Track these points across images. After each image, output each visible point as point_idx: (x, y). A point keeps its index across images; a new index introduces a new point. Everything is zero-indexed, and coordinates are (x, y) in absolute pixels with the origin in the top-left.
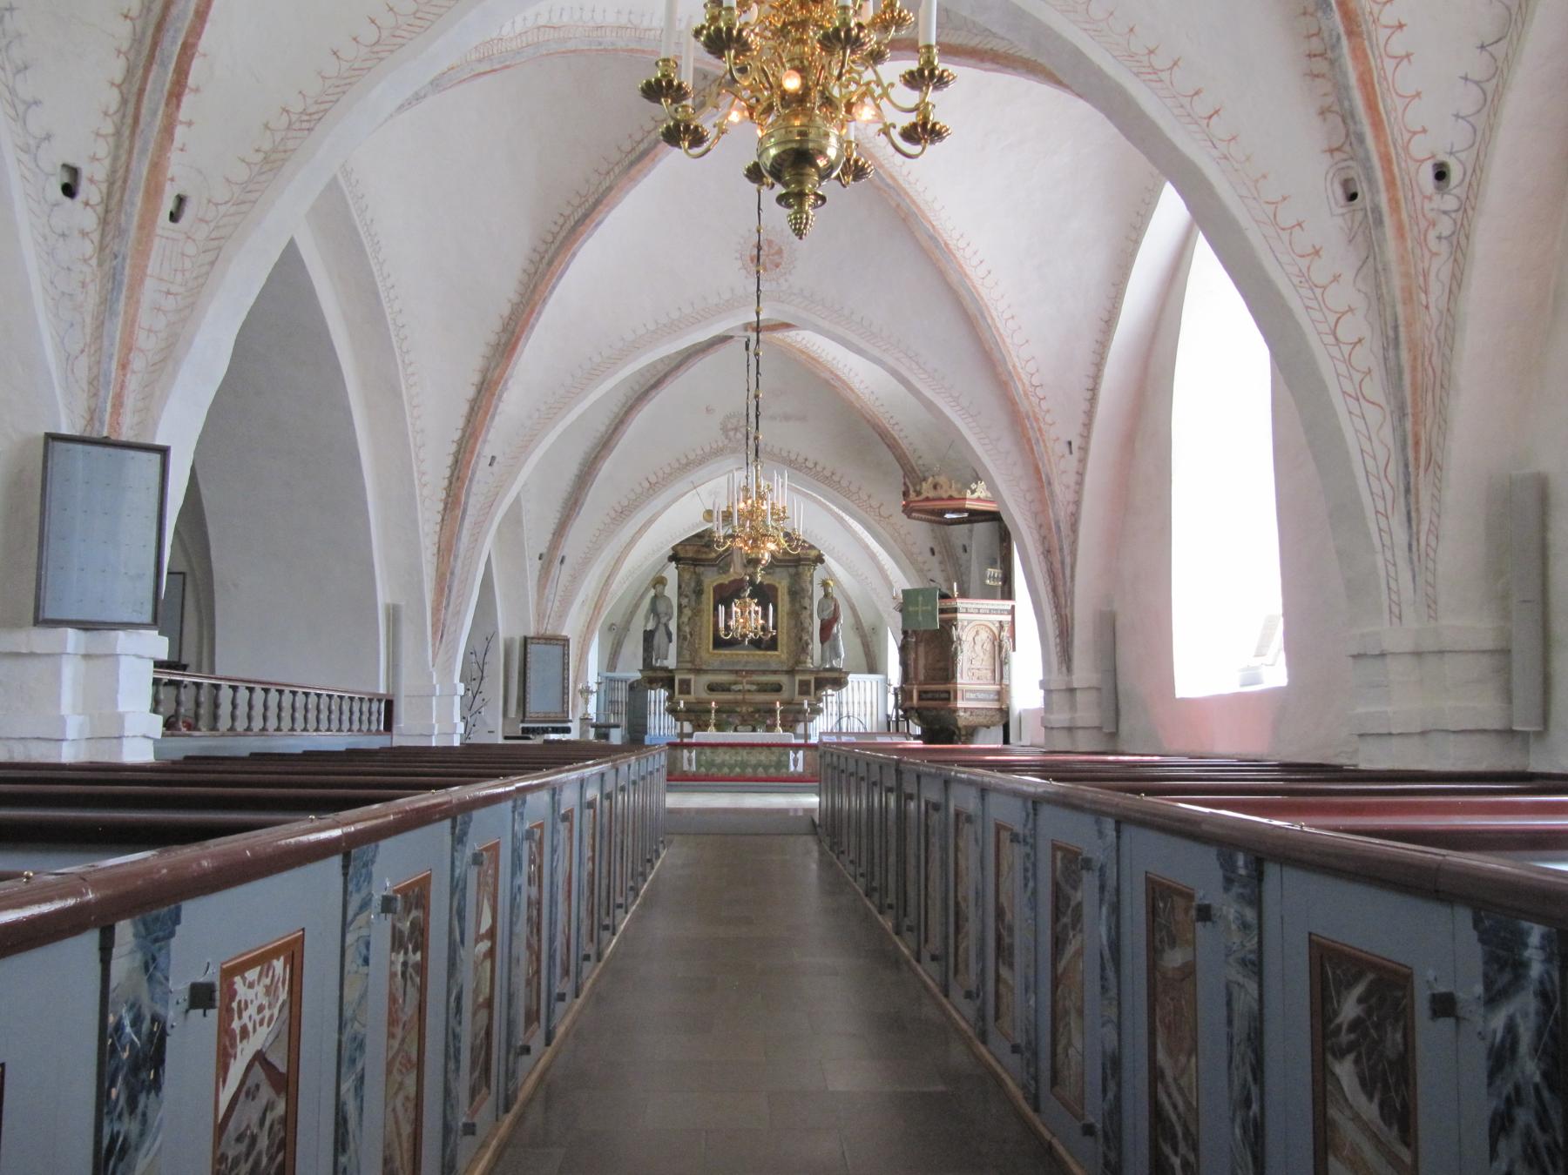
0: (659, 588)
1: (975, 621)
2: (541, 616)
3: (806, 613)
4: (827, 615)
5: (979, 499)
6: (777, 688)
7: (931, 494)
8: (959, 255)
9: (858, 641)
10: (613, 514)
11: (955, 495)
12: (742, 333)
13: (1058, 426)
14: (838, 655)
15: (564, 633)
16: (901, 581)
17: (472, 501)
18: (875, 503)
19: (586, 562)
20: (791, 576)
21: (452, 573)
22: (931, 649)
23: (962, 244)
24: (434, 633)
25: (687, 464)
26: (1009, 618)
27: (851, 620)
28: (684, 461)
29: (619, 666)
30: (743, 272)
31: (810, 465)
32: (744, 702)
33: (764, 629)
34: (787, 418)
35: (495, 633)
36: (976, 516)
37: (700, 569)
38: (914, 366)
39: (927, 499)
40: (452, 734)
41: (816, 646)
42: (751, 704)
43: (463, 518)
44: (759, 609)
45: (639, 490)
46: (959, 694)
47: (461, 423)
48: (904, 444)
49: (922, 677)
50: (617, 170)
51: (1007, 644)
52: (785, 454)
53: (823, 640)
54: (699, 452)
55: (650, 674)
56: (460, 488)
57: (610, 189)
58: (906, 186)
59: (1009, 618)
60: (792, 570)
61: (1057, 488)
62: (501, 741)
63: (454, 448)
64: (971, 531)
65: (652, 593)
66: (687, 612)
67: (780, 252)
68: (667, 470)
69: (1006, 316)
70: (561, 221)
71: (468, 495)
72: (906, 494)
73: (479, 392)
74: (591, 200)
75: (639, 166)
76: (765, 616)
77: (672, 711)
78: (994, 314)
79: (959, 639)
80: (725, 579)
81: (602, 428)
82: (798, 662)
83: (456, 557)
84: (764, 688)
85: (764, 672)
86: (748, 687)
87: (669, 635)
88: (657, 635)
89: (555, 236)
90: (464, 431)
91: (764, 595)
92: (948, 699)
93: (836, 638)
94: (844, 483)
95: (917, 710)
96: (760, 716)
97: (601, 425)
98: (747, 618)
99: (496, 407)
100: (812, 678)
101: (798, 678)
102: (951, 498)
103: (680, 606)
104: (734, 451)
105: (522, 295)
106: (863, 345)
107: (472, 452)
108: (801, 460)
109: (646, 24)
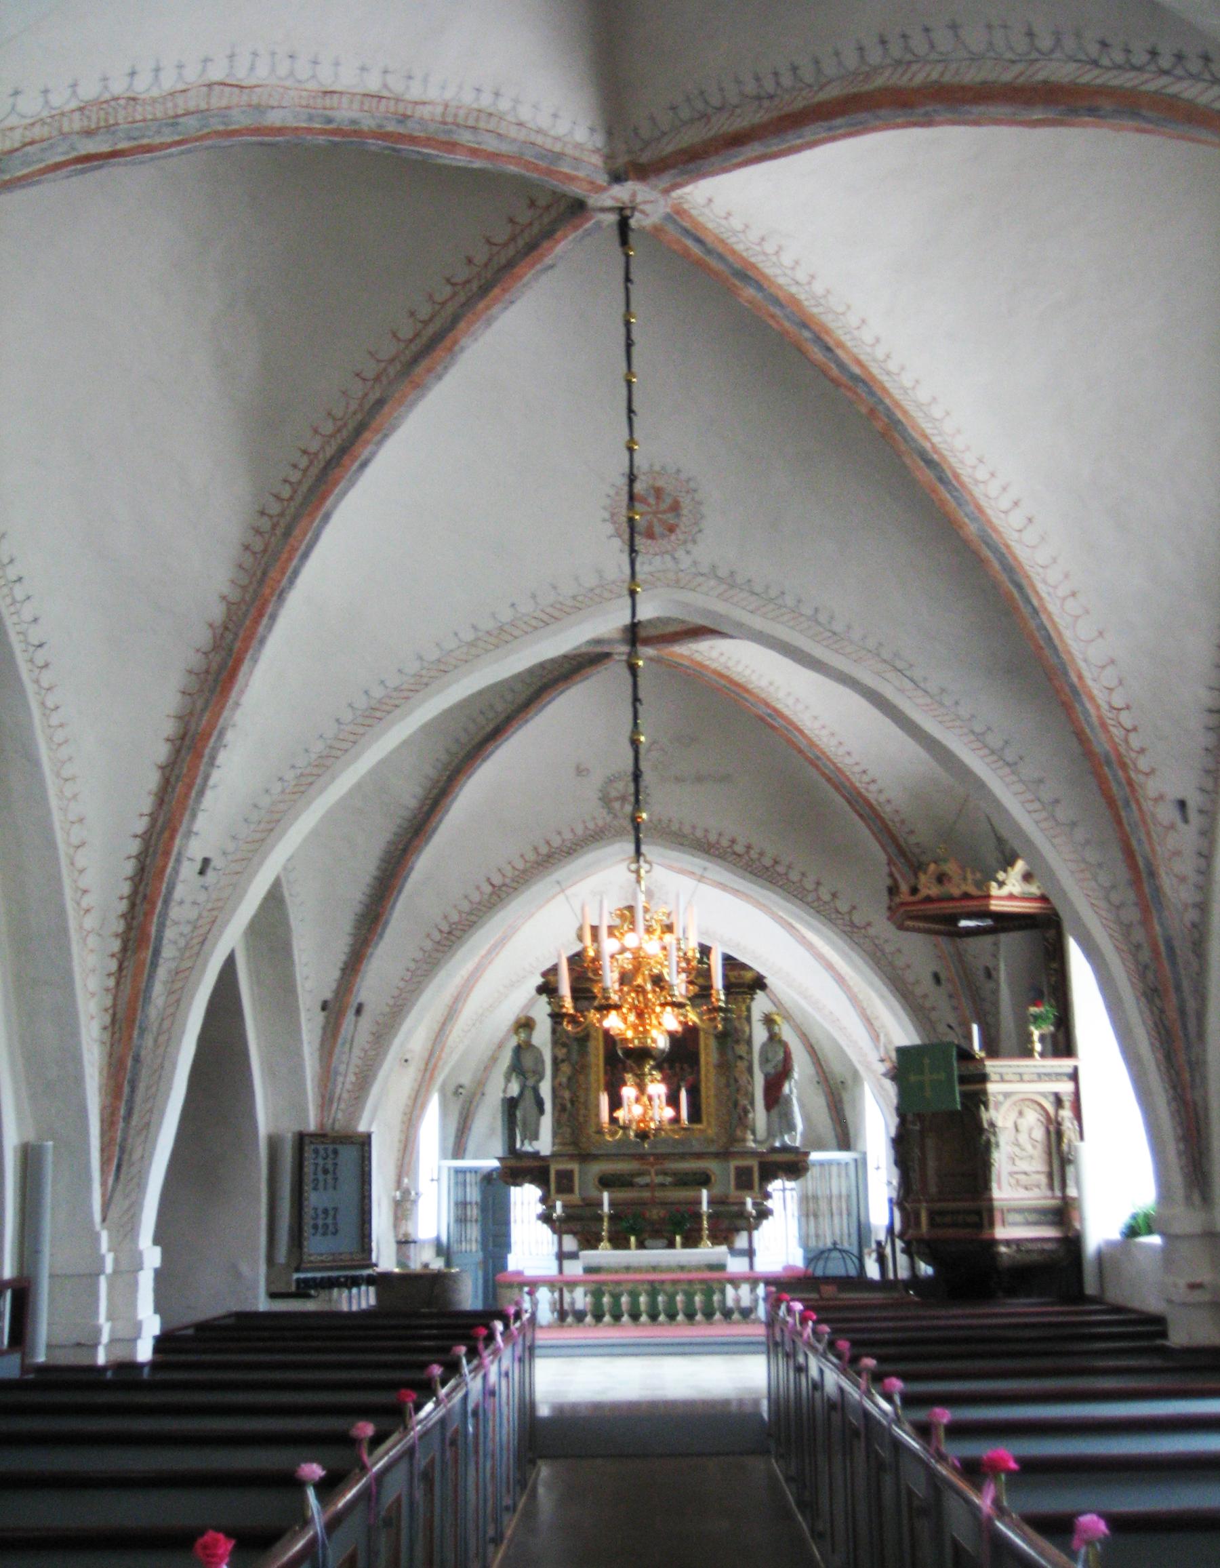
1: (1015, 1096)
2: (326, 1101)
3: (742, 1065)
5: (1011, 897)
7: (934, 891)
8: (978, 491)
10: (437, 936)
11: (972, 890)
14: (791, 1127)
15: (362, 1128)
16: (901, 1032)
17: (170, 933)
18: (844, 907)
19: (398, 1010)
21: (137, 1059)
22: (944, 1136)
23: (981, 474)
24: (105, 1163)
25: (549, 856)
27: (810, 1070)
28: (544, 850)
31: (739, 848)
32: (653, 1202)
33: (676, 1120)
34: (699, 779)
36: (1005, 922)
38: (908, 685)
39: (928, 899)
40: (133, 1340)
41: (759, 1116)
42: (663, 1204)
43: (154, 965)
46: (998, 1217)
48: (887, 811)
49: (933, 1189)
50: (392, 371)
51: (1069, 1126)
52: (699, 833)
53: (769, 1106)
54: (568, 835)
56: (148, 914)
57: (380, 402)
58: (883, 378)
61: (1167, 882)
62: (263, 1304)
63: (134, 847)
64: (996, 944)
65: (514, 1041)
66: (566, 1068)
67: (675, 507)
69: (1061, 592)
70: (304, 462)
71: (162, 927)
73: (178, 751)
74: (351, 425)
75: (425, 363)
77: (546, 1218)
79: (992, 1125)
81: (413, 803)
82: (734, 1140)
83: (143, 1031)
85: (683, 1156)
88: (522, 1105)
89: (295, 487)
90: (153, 817)
93: (788, 1100)
96: (681, 1227)
97: (408, 793)
98: (647, 1104)
99: (207, 778)
100: (754, 1163)
101: (734, 1164)
102: (966, 896)
103: (556, 1062)
104: (618, 834)
105: (244, 588)
106: (818, 651)
107: (167, 854)
108: (725, 842)
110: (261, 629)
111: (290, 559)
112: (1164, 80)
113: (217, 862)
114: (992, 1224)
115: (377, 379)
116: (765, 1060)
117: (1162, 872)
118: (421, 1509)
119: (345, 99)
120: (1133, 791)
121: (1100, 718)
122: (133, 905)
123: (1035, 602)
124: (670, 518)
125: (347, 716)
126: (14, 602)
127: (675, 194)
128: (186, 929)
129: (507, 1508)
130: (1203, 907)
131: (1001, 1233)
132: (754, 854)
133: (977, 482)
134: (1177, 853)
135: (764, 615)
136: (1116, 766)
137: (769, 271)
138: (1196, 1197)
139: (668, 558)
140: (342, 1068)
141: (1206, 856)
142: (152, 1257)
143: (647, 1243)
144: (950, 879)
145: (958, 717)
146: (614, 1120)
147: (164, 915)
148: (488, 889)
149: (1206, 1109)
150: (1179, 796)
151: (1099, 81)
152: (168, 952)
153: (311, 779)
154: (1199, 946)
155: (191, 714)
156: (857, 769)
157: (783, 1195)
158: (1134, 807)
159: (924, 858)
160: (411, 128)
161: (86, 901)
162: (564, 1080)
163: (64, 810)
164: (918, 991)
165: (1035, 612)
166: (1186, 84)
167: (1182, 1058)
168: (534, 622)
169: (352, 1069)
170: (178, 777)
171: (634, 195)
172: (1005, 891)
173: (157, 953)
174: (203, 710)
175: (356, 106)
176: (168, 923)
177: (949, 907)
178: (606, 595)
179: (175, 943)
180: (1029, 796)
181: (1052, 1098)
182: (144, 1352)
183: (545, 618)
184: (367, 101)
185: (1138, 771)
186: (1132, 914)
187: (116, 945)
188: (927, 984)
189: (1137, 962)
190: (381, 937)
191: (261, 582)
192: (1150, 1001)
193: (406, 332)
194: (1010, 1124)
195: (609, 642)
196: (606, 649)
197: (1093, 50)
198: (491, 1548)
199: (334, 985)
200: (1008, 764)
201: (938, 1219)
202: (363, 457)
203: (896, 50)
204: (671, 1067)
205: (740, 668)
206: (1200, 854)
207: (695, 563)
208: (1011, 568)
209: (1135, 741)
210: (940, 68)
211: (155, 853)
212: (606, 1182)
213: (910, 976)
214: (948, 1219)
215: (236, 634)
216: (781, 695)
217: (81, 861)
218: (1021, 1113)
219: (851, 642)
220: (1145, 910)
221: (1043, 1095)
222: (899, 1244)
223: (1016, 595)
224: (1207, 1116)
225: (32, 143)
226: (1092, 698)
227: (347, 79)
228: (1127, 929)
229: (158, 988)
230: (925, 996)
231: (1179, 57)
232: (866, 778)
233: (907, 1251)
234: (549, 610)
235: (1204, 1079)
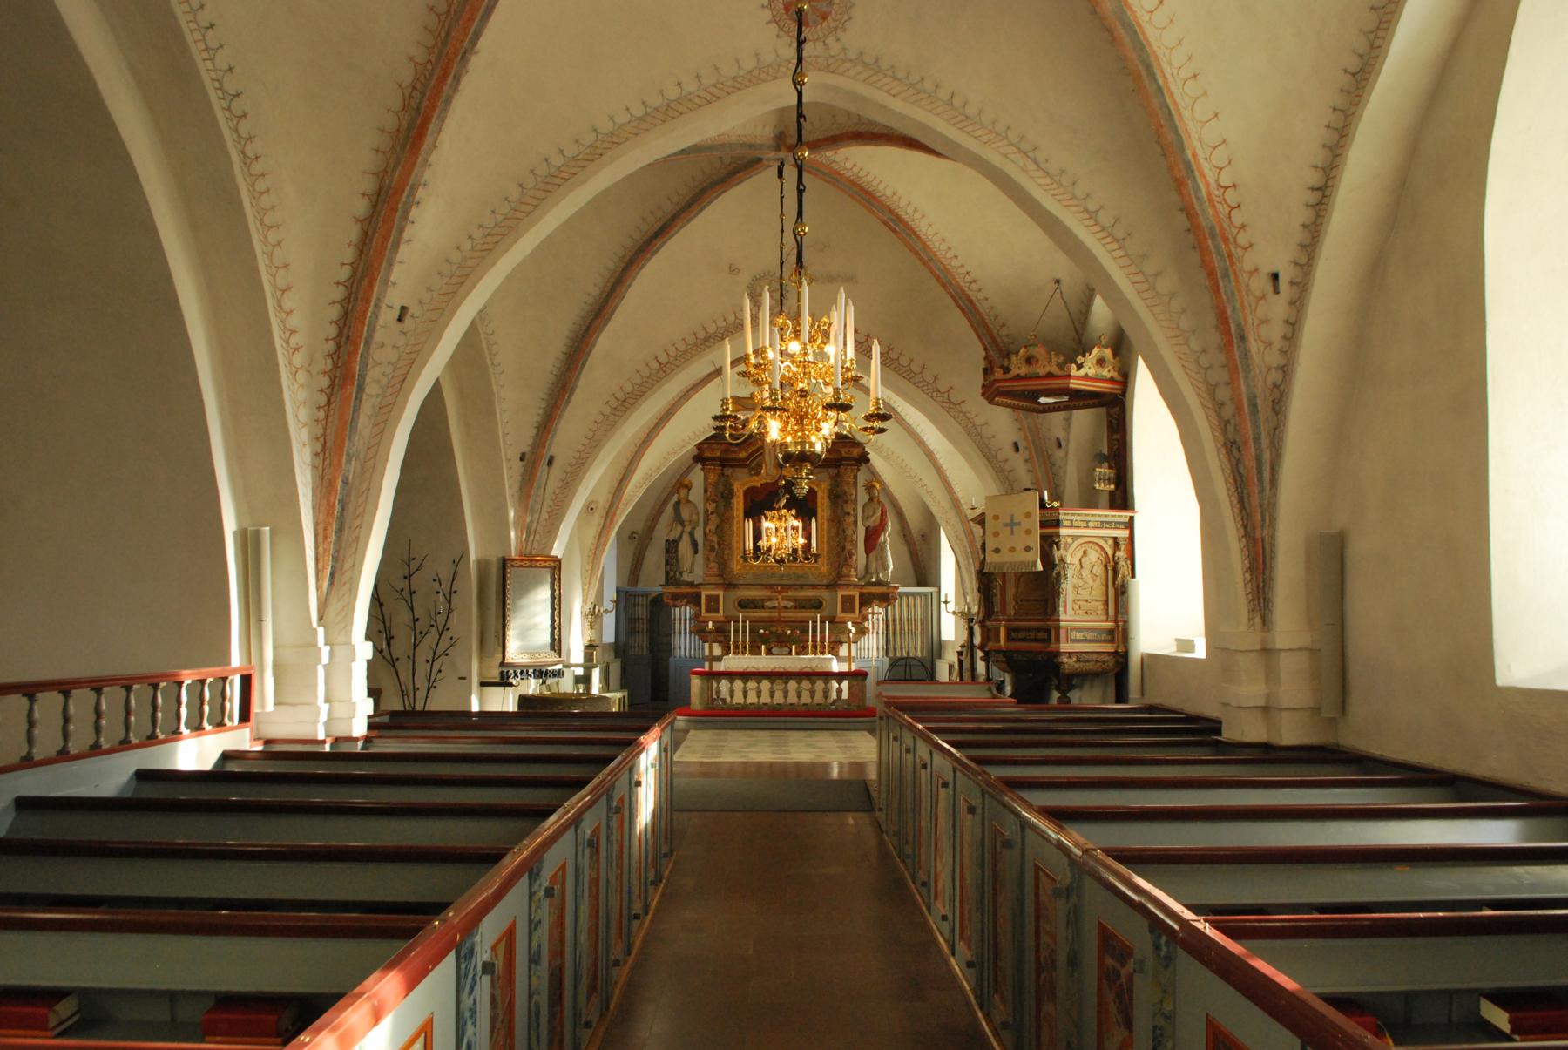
0: (683, 492)
4: (874, 520)
5: (1086, 377)
6: (817, 605)
7: (1023, 371)
10: (614, 403)
11: (1055, 370)
12: (772, 155)
13: (1266, 250)
14: (885, 567)
17: (373, 374)
20: (831, 478)
25: (707, 339)
26: (1126, 533)
28: (702, 335)
30: (773, 28)
35: (464, 554)
37: (728, 471)
38: (1032, 166)
39: (1018, 378)
41: (860, 556)
43: (359, 399)
44: (798, 524)
45: (646, 372)
47: (349, 255)
48: (983, 308)
49: (1011, 611)
51: (1124, 567)
55: (673, 589)
59: (1126, 533)
60: (833, 471)
61: (1254, 346)
64: (1068, 420)
68: (681, 347)
69: (1184, 74)
71: (365, 365)
73: (375, 206)
76: (808, 537)
78: (1167, 70)
79: (1062, 560)
80: (757, 482)
81: (595, 291)
82: (840, 575)
84: (801, 605)
85: (802, 587)
86: (784, 603)
87: (695, 545)
90: (354, 266)
91: (805, 509)
92: (1048, 640)
93: (883, 549)
95: (1004, 653)
99: (401, 231)
100: (856, 593)
101: (841, 593)
102: (1050, 375)
103: (706, 512)
105: (430, 50)
107: (367, 300)
110: (446, 88)
111: (471, 20)
113: (414, 310)
114: (1058, 640)
116: (865, 518)
117: (1251, 338)
118: (587, 872)
120: (1232, 264)
121: (1209, 194)
122: (338, 347)
123: (1161, 81)
125: (530, 182)
126: (207, 49)
128: (389, 370)
129: (665, 855)
131: (1065, 647)
134: (1265, 321)
138: (1258, 620)
142: (365, 650)
143: (774, 650)
145: (1074, 197)
146: (757, 548)
148: (655, 366)
149: (1273, 545)
152: (371, 389)
153: (497, 238)
155: (385, 171)
156: (962, 271)
157: (876, 616)
158: (1232, 277)
159: (1012, 348)
161: (294, 341)
162: (713, 527)
163: (270, 256)
164: (1000, 456)
165: (1160, 89)
167: (1255, 500)
168: (697, 100)
169: (545, 509)
170: (375, 231)
172: (1082, 372)
173: (361, 389)
174: (395, 167)
178: (763, 76)
179: (378, 381)
180: (1133, 269)
181: (1111, 542)
182: (359, 728)
183: (709, 97)
185: (1237, 245)
186: (1218, 375)
187: (325, 382)
188: (1008, 450)
189: (1219, 416)
190: (568, 402)
191: (445, 43)
192: (1229, 452)
194: (1076, 561)
195: (761, 147)
196: (758, 154)
198: (651, 888)
199: (530, 441)
200: (1117, 240)
201: (1014, 635)
205: (869, 178)
206: (1287, 322)
208: (1141, 46)
211: (356, 299)
212: (744, 605)
214: (1022, 635)
215: (423, 94)
217: (288, 303)
218: (1085, 553)
219: (983, 127)
220: (1232, 370)
221: (1103, 538)
222: (979, 654)
223: (1144, 73)
224: (1272, 551)
226: (1203, 175)
228: (1212, 390)
232: (968, 279)
233: (986, 659)
234: (711, 90)
235: (1273, 520)
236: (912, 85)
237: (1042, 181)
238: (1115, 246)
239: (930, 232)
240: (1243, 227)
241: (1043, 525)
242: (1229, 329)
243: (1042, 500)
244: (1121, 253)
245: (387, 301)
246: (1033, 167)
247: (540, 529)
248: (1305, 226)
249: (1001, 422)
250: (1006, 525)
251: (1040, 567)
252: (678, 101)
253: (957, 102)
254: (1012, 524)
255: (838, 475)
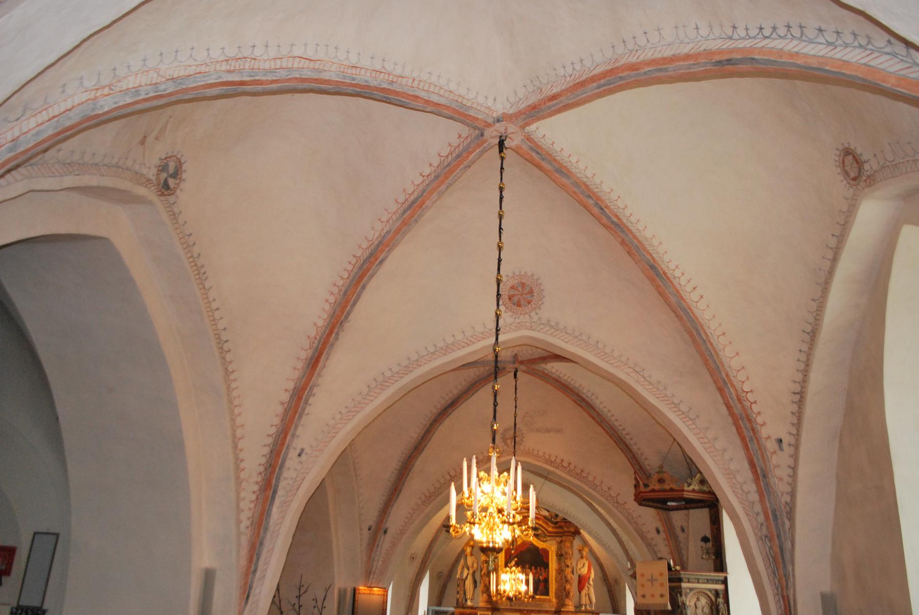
5: (694, 491)
7: (657, 487)
9: (605, 589)
10: (423, 498)
13: (772, 425)
17: (282, 484)
29: (444, 601)
31: (565, 464)
33: (527, 592)
39: (653, 491)
43: (273, 498)
50: (394, 218)
58: (629, 225)
59: (720, 587)
60: (558, 539)
61: (773, 481)
64: (688, 515)
67: (531, 292)
69: (717, 333)
71: (278, 479)
72: (636, 486)
78: (708, 331)
79: (684, 604)
81: (415, 436)
94: (590, 478)
99: (304, 409)
108: (558, 461)
109: (398, 71)
112: (768, 41)
113: (307, 450)
115: (388, 221)
119: (363, 71)
120: (754, 434)
123: (704, 337)
124: (529, 297)
127: (528, 129)
128: (291, 482)
130: (793, 494)
132: (572, 467)
133: (675, 278)
134: (777, 466)
135: (572, 344)
136: (745, 420)
137: (573, 170)
139: (527, 316)
140: (376, 558)
141: (794, 468)
144: (664, 481)
147: (280, 474)
149: (795, 600)
150: (779, 437)
151: (733, 46)
152: (280, 492)
154: (791, 515)
160: (395, 87)
164: (649, 536)
166: (778, 41)
171: (506, 129)
172: (691, 488)
173: (275, 492)
175: (368, 74)
176: (282, 478)
177: (661, 495)
184: (374, 73)
188: (653, 533)
190: (398, 497)
193: (401, 200)
194: (692, 604)
197: (729, 32)
200: (691, 419)
202: (381, 258)
203: (630, 46)
204: (536, 569)
205: (566, 378)
207: (540, 319)
209: (755, 408)
210: (652, 51)
213: (644, 529)
216: (585, 391)
218: (698, 599)
219: (614, 358)
221: (710, 590)
225: (200, 73)
227: (366, 62)
229: (275, 510)
230: (652, 539)
231: (774, 28)
236: (576, 337)
237: (648, 387)
238: (690, 422)
239: (601, 406)
240: (759, 413)
241: (670, 580)
242: (756, 471)
243: (669, 565)
244: (694, 426)
245: (294, 445)
246: (642, 379)
247: (377, 572)
248: (793, 413)
249: (649, 517)
250: (648, 580)
251: (669, 608)
252: (452, 344)
253: (600, 345)
254: (652, 580)
255: (561, 541)
